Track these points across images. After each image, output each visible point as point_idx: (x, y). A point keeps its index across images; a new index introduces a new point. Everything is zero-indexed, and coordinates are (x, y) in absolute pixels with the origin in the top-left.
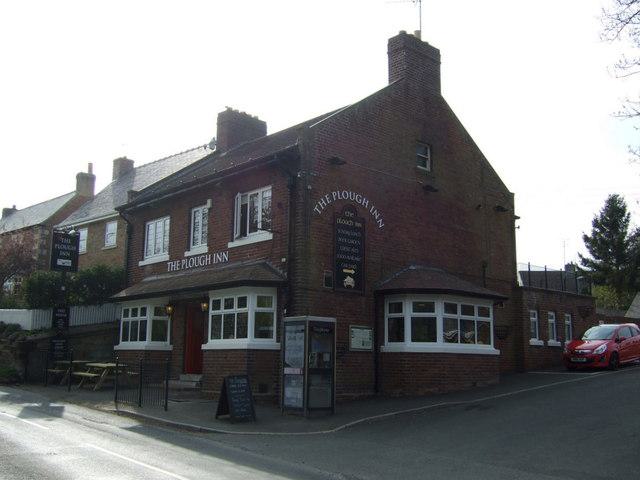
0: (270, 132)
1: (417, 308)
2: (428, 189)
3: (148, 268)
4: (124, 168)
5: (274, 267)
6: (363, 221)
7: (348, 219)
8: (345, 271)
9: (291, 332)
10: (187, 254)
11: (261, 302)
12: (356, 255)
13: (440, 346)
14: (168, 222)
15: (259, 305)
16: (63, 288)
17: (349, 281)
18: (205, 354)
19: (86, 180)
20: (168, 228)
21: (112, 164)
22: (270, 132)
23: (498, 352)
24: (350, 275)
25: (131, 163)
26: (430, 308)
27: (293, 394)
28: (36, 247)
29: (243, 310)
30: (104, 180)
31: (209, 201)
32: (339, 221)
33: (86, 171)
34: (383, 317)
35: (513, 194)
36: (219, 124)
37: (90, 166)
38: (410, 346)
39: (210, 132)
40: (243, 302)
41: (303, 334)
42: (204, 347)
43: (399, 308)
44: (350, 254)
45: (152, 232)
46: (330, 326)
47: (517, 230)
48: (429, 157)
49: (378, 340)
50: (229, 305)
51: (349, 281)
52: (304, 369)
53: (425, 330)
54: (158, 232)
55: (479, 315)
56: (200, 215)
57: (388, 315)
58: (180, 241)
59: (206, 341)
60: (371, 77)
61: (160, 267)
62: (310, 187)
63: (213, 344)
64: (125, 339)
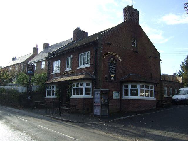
0: (89, 35)
1: (132, 86)
2: (135, 52)
4: (46, 46)
7: (112, 60)
8: (111, 76)
10: (65, 71)
11: (87, 85)
12: (114, 71)
14: (60, 61)
17: (112, 78)
19: (36, 50)
20: (60, 63)
22: (89, 35)
23: (155, 99)
26: (136, 86)
27: (97, 111)
30: (41, 49)
33: (36, 47)
38: (130, 97)
44: (113, 71)
49: (121, 95)
50: (50, 88)
51: (112, 78)
54: (57, 64)
57: (124, 88)
60: (118, 19)
61: (57, 75)
62: (101, 51)
64: (48, 95)
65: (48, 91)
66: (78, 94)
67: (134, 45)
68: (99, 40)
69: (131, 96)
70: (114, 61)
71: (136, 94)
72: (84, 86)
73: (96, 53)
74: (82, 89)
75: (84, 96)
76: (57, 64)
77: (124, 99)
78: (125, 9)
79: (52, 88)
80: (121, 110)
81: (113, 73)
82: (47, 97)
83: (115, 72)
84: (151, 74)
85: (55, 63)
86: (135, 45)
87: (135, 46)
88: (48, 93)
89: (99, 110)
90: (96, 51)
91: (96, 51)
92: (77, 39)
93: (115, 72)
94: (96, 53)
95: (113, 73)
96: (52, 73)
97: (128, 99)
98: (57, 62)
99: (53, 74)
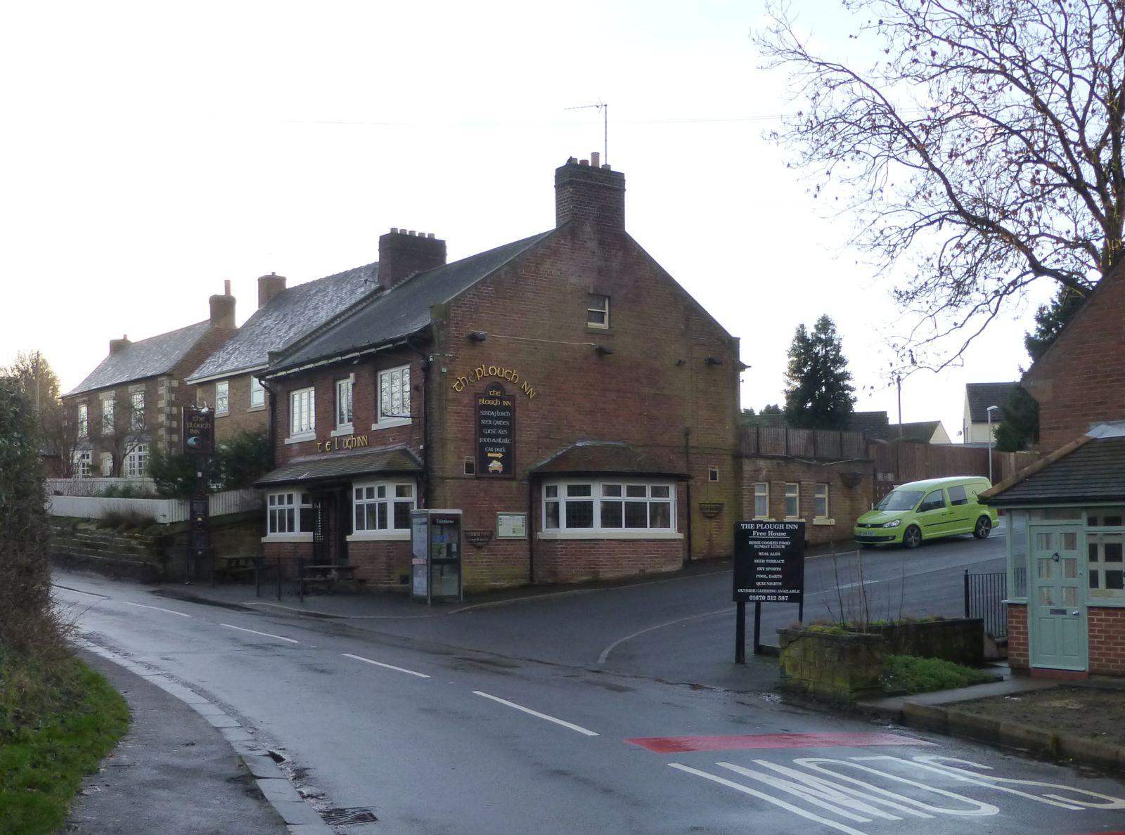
0: (452, 256)
1: (572, 491)
2: (601, 352)
3: (296, 447)
4: (272, 291)
5: (414, 453)
6: (512, 398)
7: (494, 398)
8: (489, 455)
9: (417, 524)
10: (333, 433)
11: (400, 492)
12: (503, 436)
13: (597, 531)
14: (313, 393)
15: (398, 495)
16: (200, 474)
17: (495, 465)
18: (350, 546)
19: (222, 306)
20: (313, 400)
21: (257, 283)
22: (452, 256)
23: (681, 536)
24: (497, 459)
25: (281, 281)
26: (586, 491)
27: (420, 585)
28: (162, 418)
29: (382, 500)
30: (246, 308)
31: (352, 375)
32: (482, 402)
33: (222, 292)
34: (541, 501)
35: (738, 339)
36: (380, 250)
37: (228, 285)
38: (564, 532)
39: (371, 255)
40: (382, 492)
41: (426, 526)
42: (264, 540)
43: (552, 491)
44: (497, 436)
45: (296, 404)
46: (456, 518)
47: (741, 383)
48: (607, 311)
49: (533, 525)
50: (370, 493)
51: (495, 465)
52: (427, 561)
53: (580, 516)
54: (303, 407)
55: (629, 495)
56: (346, 387)
57: (545, 499)
58: (326, 414)
59: (350, 532)
61: (306, 447)
62: (444, 370)
63: (358, 535)
64: (273, 530)
65: (360, 507)
66: (282, 529)
67: (602, 321)
68: (435, 328)
69: (568, 526)
70: (500, 398)
71: (586, 521)
72: (391, 498)
73: (428, 378)
74: (383, 507)
75: (392, 532)
76: (305, 402)
77: (545, 540)
78: (560, 173)
79: (286, 501)
80: (532, 579)
81: (499, 445)
82: (272, 537)
83: (506, 441)
84: (687, 434)
85: (297, 398)
86: (606, 318)
87: (605, 326)
88: (273, 518)
89: (426, 579)
90: (427, 369)
91: (427, 369)
92: (394, 281)
93: (506, 441)
94: (428, 378)
95: (499, 445)
96: (287, 441)
97: (557, 540)
98: (305, 395)
99: (291, 444)
